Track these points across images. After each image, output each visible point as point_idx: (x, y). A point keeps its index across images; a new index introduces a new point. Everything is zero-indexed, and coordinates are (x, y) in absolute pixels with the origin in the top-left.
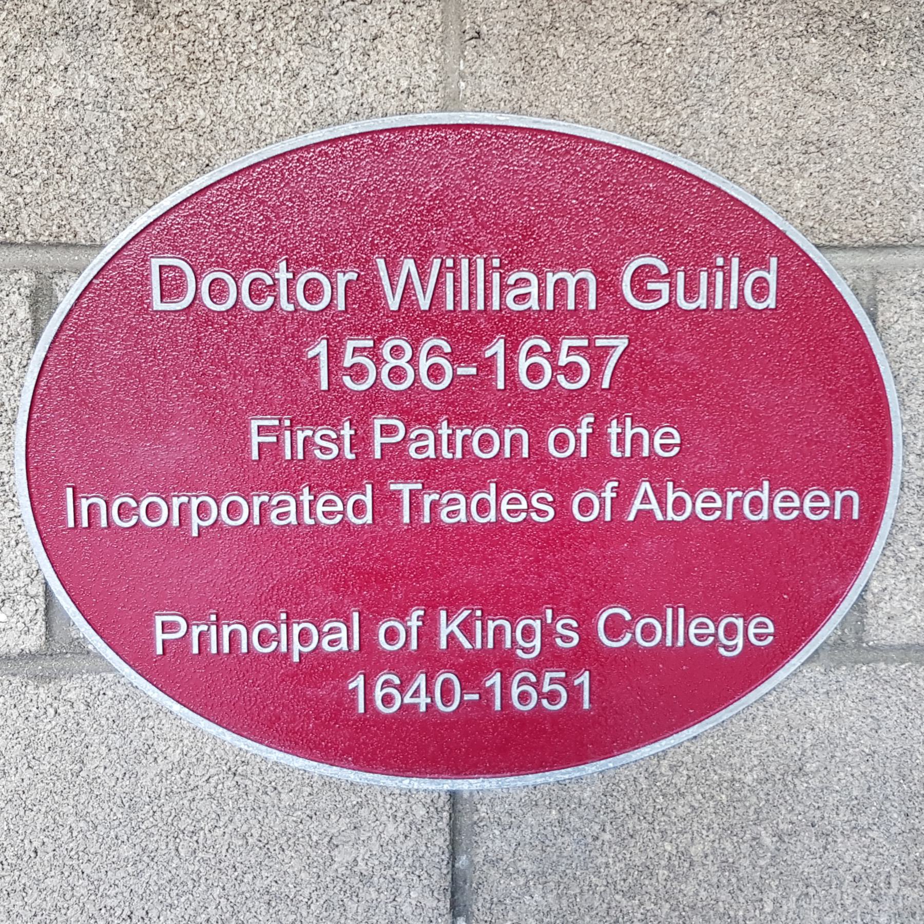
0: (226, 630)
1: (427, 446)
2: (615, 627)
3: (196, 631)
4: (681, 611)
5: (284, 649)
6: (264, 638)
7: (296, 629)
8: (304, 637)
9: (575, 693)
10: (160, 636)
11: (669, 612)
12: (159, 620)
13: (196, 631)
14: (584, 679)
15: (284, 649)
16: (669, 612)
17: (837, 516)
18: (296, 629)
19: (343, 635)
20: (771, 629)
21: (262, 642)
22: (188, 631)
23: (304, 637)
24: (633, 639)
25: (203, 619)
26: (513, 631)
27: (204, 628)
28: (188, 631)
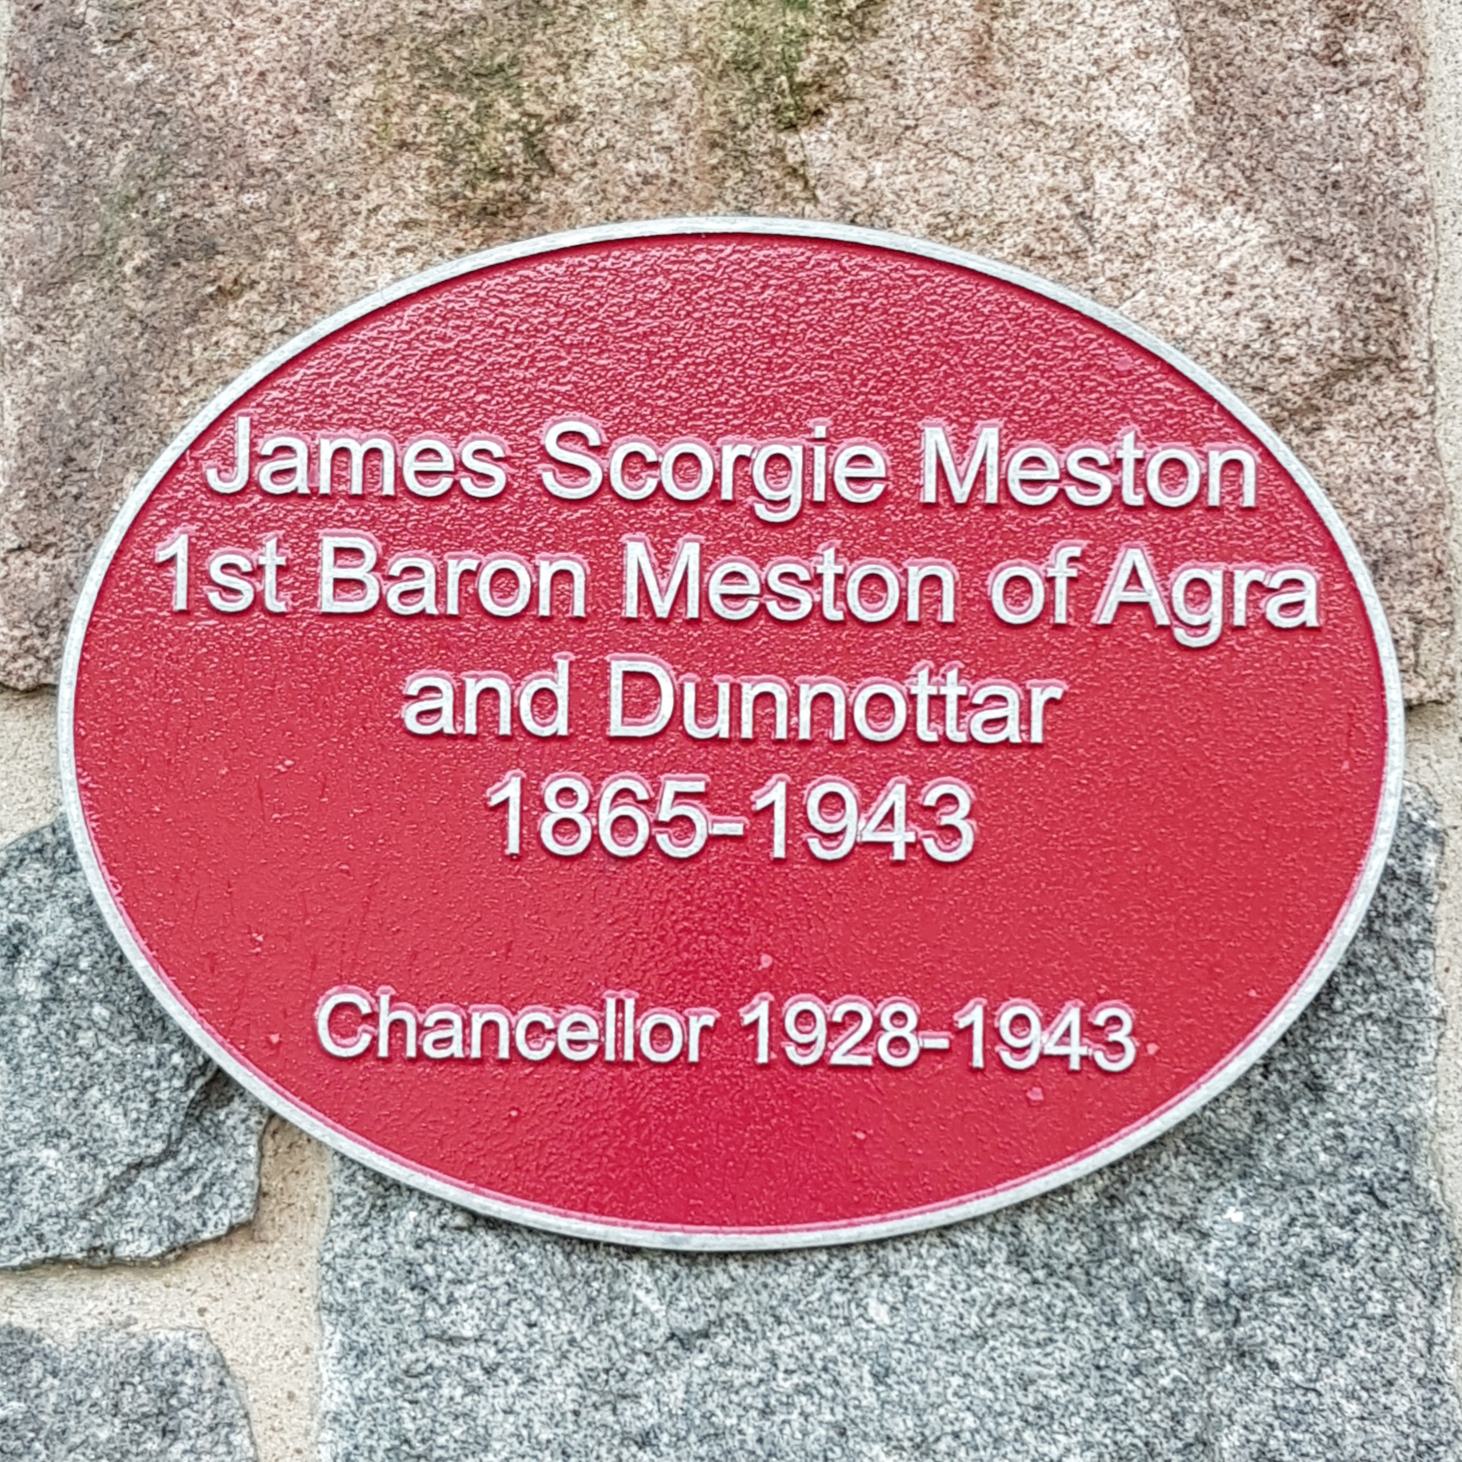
4: (630, 1005)
11: (611, 1005)
16: (611, 1005)
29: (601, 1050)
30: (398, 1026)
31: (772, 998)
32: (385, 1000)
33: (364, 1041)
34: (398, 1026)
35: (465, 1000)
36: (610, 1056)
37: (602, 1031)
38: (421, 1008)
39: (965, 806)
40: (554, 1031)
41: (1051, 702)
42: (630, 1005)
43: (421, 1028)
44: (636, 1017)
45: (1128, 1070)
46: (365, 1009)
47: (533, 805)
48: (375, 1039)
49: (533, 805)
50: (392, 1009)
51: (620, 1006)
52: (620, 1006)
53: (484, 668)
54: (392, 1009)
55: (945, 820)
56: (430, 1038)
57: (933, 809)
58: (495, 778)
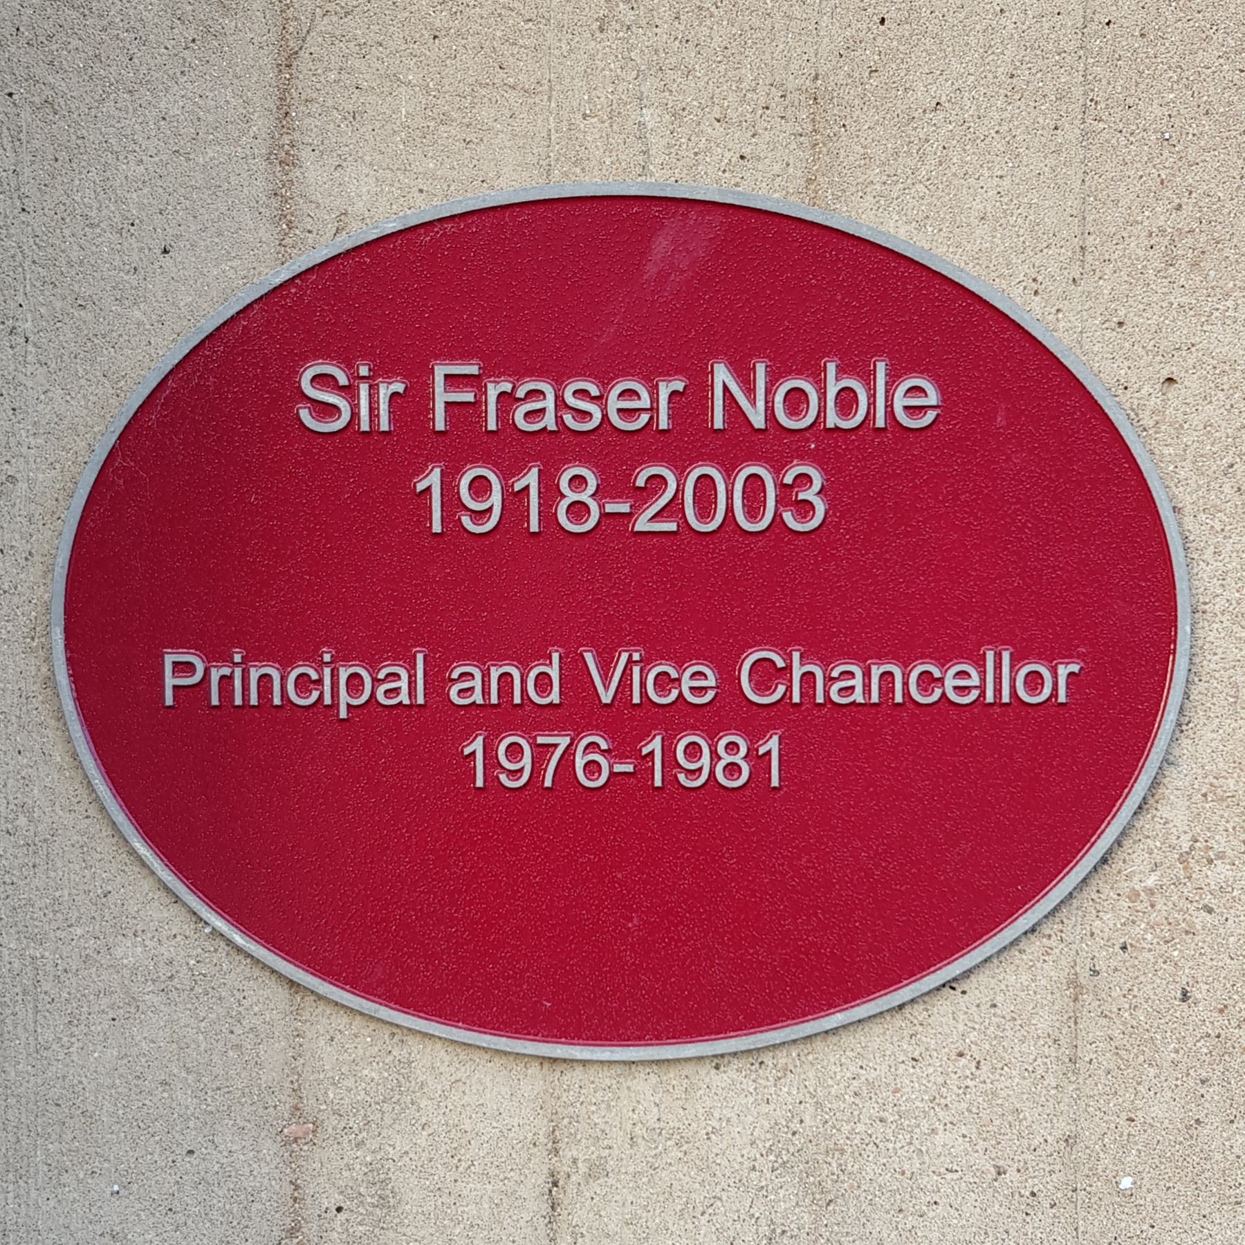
0: (254, 675)
1: (543, 411)
2: (766, 675)
3: (215, 675)
4: (1006, 656)
5: (328, 700)
6: (303, 684)
7: (344, 675)
8: (355, 683)
9: (759, 762)
10: (170, 681)
11: (990, 656)
12: (169, 660)
13: (215, 675)
14: (772, 745)
15: (328, 700)
16: (990, 656)
17: (664, 423)
18: (344, 675)
19: (403, 684)
20: (711, 682)
21: (762, 686)
22: (207, 672)
23: (355, 683)
24: (944, 695)
25: (227, 659)
26: (283, 679)
27: (226, 671)
28: (207, 672)
29: (983, 694)
30: (808, 678)
31: (1012, 650)
32: (796, 656)
33: (315, 694)
34: (808, 678)
35: (484, 658)
36: (990, 697)
37: (983, 680)
38: (826, 663)
39: (818, 482)
40: (679, 680)
41: (674, 393)
42: (1006, 656)
43: (829, 680)
44: (1012, 666)
45: (673, 703)
46: (780, 663)
47: (550, 493)
48: (322, 694)
49: (550, 493)
50: (802, 665)
51: (998, 657)
52: (998, 657)
53: (670, 375)
54: (802, 665)
55: (801, 496)
56: (382, 688)
57: (791, 487)
58: (420, 470)
